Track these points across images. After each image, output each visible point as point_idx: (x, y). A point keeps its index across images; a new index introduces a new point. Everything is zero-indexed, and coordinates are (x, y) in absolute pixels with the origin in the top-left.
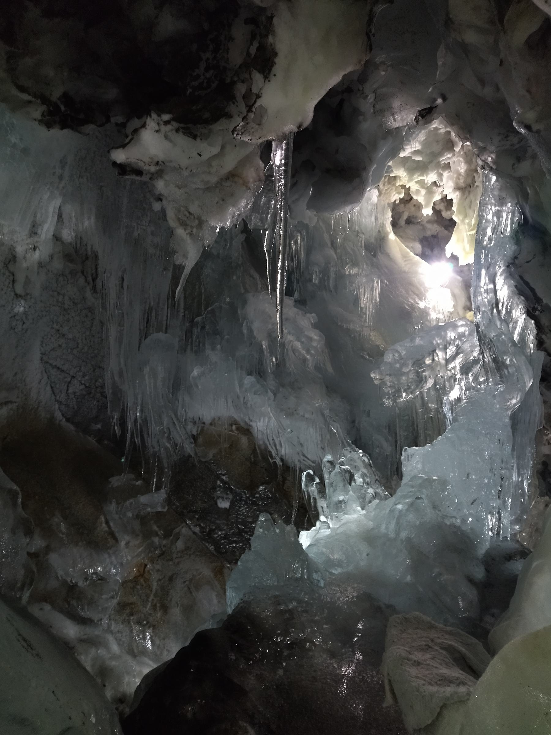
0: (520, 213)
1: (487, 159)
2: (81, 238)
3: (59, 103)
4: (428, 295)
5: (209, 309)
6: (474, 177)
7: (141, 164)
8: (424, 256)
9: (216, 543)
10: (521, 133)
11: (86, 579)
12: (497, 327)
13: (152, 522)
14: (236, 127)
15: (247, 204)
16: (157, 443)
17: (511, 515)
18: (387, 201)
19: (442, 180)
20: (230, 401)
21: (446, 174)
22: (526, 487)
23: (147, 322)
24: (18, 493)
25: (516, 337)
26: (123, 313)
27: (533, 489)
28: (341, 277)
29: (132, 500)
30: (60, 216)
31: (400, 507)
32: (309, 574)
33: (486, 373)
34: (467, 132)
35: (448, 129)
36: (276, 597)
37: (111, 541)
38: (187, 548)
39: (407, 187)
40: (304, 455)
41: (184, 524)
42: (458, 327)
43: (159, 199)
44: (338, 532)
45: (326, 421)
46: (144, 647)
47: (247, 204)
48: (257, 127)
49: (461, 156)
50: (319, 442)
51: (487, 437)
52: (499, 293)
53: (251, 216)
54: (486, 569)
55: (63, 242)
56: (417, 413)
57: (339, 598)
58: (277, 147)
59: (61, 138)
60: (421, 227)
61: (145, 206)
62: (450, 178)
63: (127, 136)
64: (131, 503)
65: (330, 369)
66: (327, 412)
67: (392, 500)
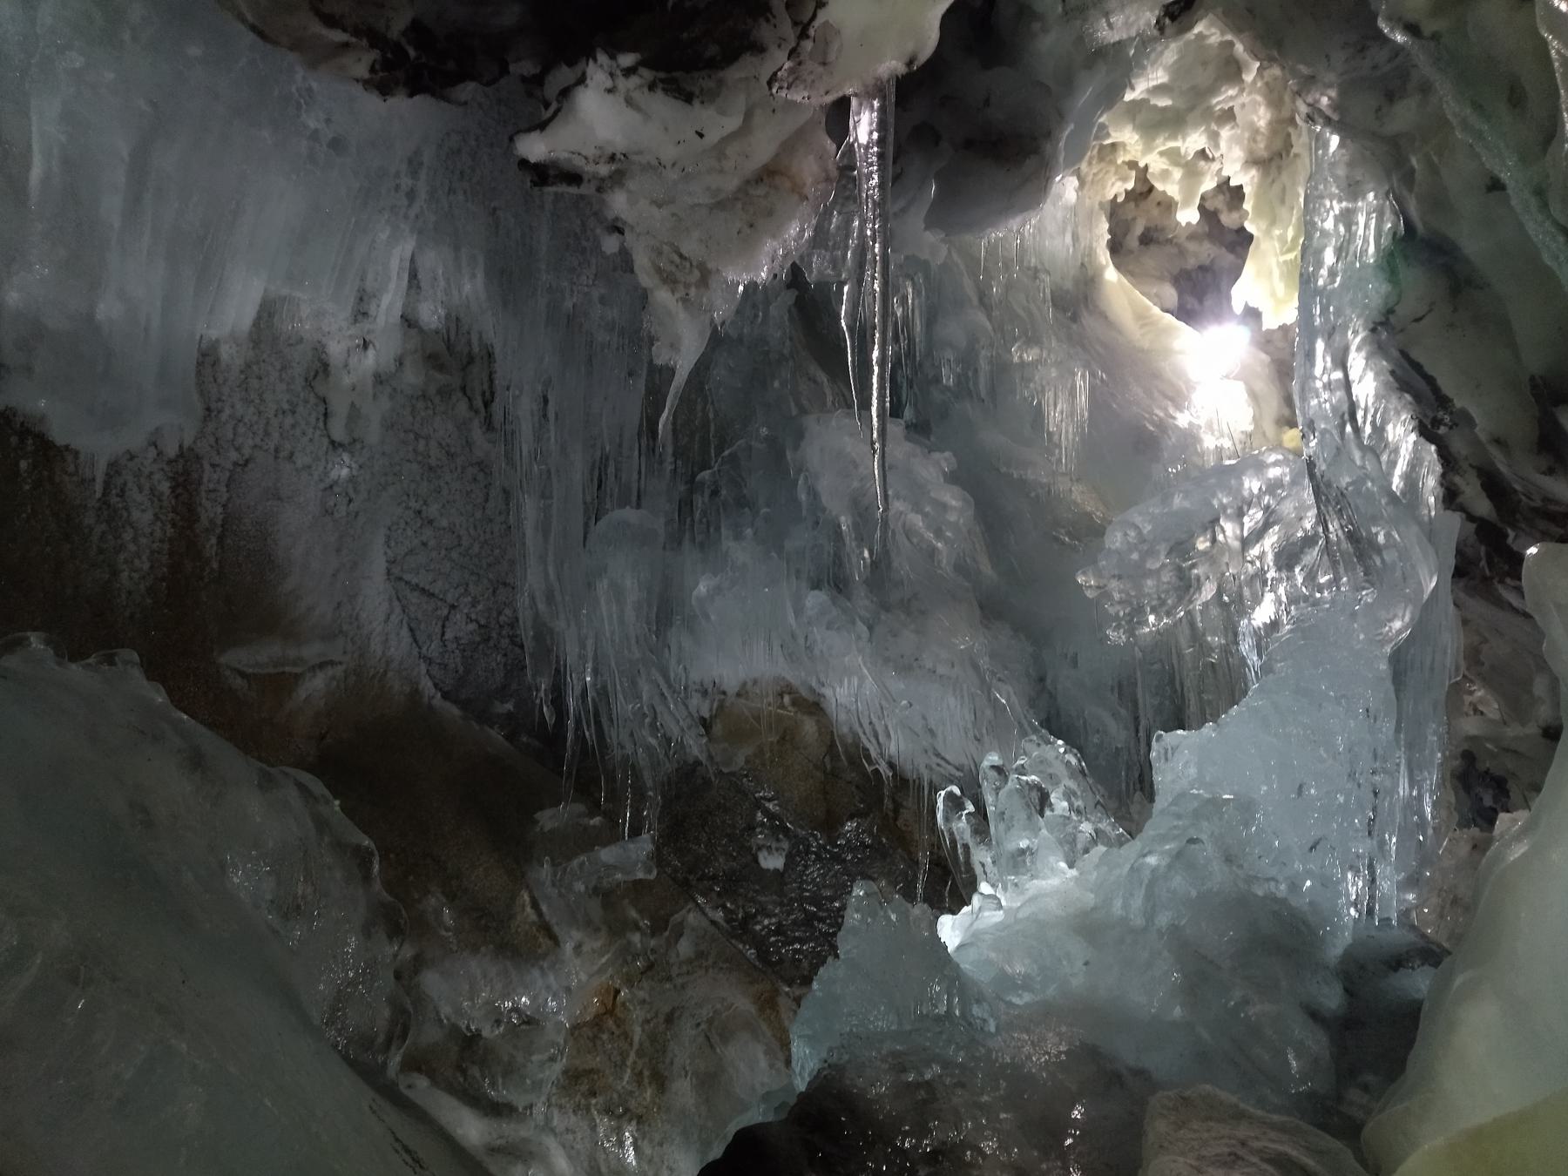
0: (1396, 214)
1: (1318, 101)
2: (458, 319)
3: (403, 41)
4: (1196, 398)
5: (726, 453)
6: (1289, 135)
7: (579, 162)
8: (1185, 314)
9: (760, 944)
10: (1395, 42)
11: (498, 1022)
12: (1353, 461)
13: (626, 901)
14: (775, 74)
15: (802, 230)
16: (629, 739)
17: (1398, 870)
18: (1098, 198)
19: (1217, 146)
20: (776, 648)
21: (1225, 133)
22: (1428, 810)
23: (599, 487)
24: (372, 854)
25: (1397, 483)
26: (549, 471)
27: (1444, 813)
28: (1002, 369)
29: (583, 858)
30: (413, 275)
31: (1152, 860)
32: (965, 1005)
33: (1334, 564)
34: (1273, 40)
35: (1229, 37)
36: (894, 1054)
37: (545, 942)
38: (700, 955)
39: (1142, 165)
40: (938, 755)
41: (691, 905)
42: (1268, 466)
43: (617, 228)
44: (1020, 915)
45: (983, 680)
46: (621, 1161)
47: (802, 230)
48: (821, 69)
49: (1259, 91)
50: (970, 726)
51: (1339, 704)
52: (1355, 390)
53: (810, 255)
54: (1346, 990)
55: (421, 331)
56: (1180, 656)
57: (1029, 1057)
58: (861, 105)
59: (408, 118)
60: (1174, 250)
61: (584, 243)
62: (1234, 140)
63: (547, 105)
64: (582, 865)
65: (986, 568)
66: (984, 662)
67: (1136, 845)
